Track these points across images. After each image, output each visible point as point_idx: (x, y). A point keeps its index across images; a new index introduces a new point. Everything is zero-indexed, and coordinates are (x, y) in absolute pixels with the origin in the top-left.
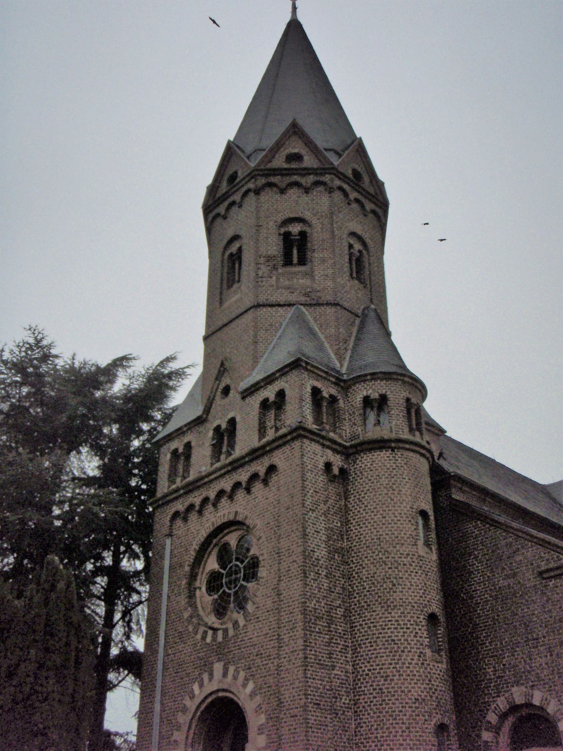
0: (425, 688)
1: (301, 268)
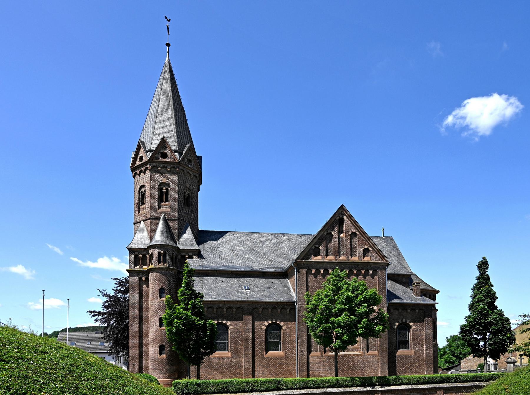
1: (167, 203)
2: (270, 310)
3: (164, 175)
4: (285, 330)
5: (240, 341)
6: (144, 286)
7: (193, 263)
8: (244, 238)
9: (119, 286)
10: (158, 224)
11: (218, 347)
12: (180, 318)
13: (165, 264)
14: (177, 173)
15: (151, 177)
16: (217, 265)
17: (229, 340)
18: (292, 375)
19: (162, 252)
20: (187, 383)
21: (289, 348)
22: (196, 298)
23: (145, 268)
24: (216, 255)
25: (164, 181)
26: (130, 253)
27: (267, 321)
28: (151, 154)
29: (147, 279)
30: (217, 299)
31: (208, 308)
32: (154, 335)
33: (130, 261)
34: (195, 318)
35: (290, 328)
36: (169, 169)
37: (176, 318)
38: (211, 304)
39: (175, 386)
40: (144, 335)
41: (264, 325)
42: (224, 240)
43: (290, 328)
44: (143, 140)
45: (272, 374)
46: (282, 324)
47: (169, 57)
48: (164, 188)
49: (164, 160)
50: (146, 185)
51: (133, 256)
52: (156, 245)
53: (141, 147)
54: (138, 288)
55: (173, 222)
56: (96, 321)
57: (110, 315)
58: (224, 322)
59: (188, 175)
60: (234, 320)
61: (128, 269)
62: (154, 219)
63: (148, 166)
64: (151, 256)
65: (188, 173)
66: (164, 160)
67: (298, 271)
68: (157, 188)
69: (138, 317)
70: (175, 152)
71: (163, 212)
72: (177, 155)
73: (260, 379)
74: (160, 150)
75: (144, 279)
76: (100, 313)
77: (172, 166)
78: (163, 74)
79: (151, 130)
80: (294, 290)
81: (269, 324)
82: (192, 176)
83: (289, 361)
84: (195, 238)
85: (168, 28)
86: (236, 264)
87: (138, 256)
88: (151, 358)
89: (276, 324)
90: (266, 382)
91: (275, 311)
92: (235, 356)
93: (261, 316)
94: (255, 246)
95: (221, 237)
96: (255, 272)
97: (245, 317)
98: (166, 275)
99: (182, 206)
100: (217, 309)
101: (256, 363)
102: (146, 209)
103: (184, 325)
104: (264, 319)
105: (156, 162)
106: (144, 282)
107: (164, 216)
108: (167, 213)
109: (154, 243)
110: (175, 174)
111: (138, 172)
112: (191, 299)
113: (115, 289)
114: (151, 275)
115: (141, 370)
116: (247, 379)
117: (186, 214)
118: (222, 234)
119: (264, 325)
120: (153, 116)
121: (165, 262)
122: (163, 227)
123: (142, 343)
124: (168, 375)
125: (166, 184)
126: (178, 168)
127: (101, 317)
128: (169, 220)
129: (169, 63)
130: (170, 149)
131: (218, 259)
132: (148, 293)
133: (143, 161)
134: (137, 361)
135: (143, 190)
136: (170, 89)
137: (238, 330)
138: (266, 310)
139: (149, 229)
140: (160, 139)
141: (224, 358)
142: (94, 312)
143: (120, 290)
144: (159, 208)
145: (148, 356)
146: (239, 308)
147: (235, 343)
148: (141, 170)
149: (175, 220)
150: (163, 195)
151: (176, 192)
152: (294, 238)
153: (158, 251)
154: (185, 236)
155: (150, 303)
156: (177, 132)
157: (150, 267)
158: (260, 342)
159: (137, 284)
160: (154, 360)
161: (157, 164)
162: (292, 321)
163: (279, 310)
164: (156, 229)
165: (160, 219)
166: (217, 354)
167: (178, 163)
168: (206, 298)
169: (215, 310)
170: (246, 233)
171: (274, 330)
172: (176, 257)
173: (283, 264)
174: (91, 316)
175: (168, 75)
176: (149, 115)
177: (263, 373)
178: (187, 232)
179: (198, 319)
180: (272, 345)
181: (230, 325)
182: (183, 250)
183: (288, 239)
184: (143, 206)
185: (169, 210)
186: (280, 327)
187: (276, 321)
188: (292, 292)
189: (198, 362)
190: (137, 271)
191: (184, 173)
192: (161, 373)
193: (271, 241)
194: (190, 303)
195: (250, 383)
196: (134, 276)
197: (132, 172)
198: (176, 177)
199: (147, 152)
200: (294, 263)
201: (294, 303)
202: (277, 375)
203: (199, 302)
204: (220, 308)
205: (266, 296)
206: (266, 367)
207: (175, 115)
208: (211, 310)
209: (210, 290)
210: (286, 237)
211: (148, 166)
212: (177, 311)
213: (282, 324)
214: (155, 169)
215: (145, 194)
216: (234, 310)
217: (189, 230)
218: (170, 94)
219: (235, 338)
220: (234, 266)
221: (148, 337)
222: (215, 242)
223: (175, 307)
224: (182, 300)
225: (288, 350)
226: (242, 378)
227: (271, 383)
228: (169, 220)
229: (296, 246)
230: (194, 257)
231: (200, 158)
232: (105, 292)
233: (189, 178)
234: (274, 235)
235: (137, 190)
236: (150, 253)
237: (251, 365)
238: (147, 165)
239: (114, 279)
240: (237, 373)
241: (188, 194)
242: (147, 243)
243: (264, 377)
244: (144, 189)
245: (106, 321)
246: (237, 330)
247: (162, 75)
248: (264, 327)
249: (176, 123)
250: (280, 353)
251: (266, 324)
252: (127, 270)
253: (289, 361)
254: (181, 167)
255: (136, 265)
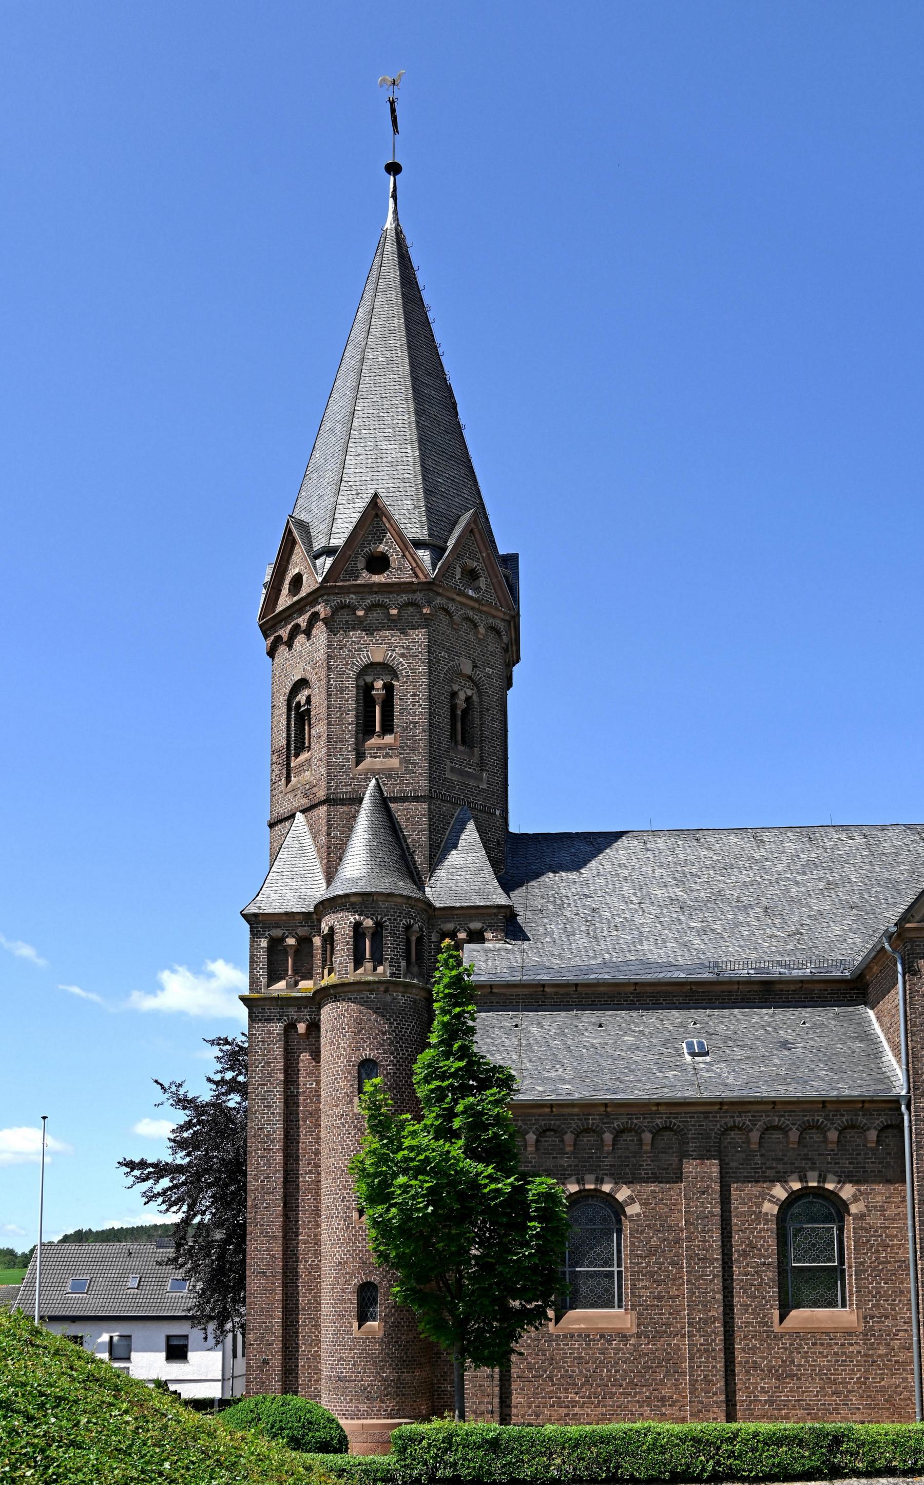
0: (348, 1251)
1: (389, 739)
2: (794, 1135)
3: (378, 636)
4: (861, 1217)
5: (674, 1264)
6: (305, 1057)
7: (488, 960)
8: (685, 851)
9: (231, 1068)
10: (355, 817)
11: (584, 1290)
12: (420, 1171)
13: (380, 969)
14: (427, 622)
15: (330, 645)
16: (577, 961)
17: (627, 1262)
18: (897, 1412)
19: (369, 923)
20: (449, 1439)
21: (878, 1294)
22: (484, 1085)
23: (307, 986)
24: (578, 925)
25: (379, 658)
26: (254, 935)
27: (782, 1179)
28: (329, 561)
29: (314, 1027)
30: (577, 1096)
31: (542, 1133)
32: (340, 1241)
33: (252, 962)
34: (481, 1167)
35: (883, 1209)
36: (394, 612)
37: (405, 1172)
38: (553, 1118)
39: (402, 1450)
40: (302, 1247)
41: (773, 1199)
42: (608, 867)
43: (883, 1209)
44: (303, 516)
45: (808, 1408)
46: (847, 1192)
47: (395, 211)
48: (379, 684)
49: (376, 579)
50: (313, 678)
51: (264, 943)
52: (347, 896)
53: (294, 542)
54: (280, 1065)
55: (412, 805)
56: (150, 1197)
57: (198, 1176)
58: (607, 1188)
59: (466, 626)
60: (646, 1180)
61: (247, 993)
62: (342, 802)
63: (322, 609)
64: (329, 939)
65: (467, 619)
66: (376, 579)
67: (910, 970)
68: (350, 684)
69: (280, 1175)
70: (418, 544)
71: (373, 773)
72: (424, 555)
73: (752, 1427)
74: (362, 546)
75: (302, 1027)
76: (161, 1170)
77: (405, 598)
78: (375, 273)
79: (330, 476)
80: (895, 1048)
81: (794, 1197)
82: (482, 630)
83: (882, 1350)
84: (495, 864)
85: (393, 110)
86: (653, 952)
87: (282, 942)
88: (327, 1333)
89: (820, 1193)
90: (778, 1440)
91: (817, 1137)
92: (652, 1329)
93: (758, 1160)
94: (731, 884)
95: (593, 856)
96: (730, 982)
97: (691, 1167)
98: (381, 1010)
99: (445, 744)
100: (578, 1135)
101: (739, 1357)
102: (313, 768)
103: (433, 1195)
104: (769, 1173)
105: (347, 590)
106: (302, 1042)
107: (378, 786)
108: (389, 776)
109: (338, 889)
110: (418, 637)
111: (284, 633)
112: (465, 1090)
113: (217, 1078)
114: (328, 1013)
115: (289, 1382)
116: (696, 1427)
117: (461, 773)
118: (598, 842)
119: (773, 1199)
120: (339, 427)
121: (378, 960)
122: (374, 829)
123: (297, 1275)
124: (390, 1405)
125: (385, 668)
126: (429, 602)
127: (165, 1183)
128: (395, 799)
129: (398, 233)
130: (400, 535)
131: (581, 941)
132: (318, 1083)
133: (303, 593)
134: (277, 1346)
135: (301, 697)
136: (399, 322)
137: (664, 1218)
138: (776, 1136)
139: (323, 839)
140: (361, 505)
141: (606, 1337)
142: (143, 1164)
143: (234, 1079)
144: (360, 757)
145: (317, 1326)
146: (666, 1128)
147: (652, 1274)
148: (297, 626)
149: (416, 799)
150: (373, 710)
151: (423, 695)
152: (891, 841)
153: (352, 918)
154: (454, 858)
155: (324, 1121)
156: (426, 471)
157: (323, 983)
158: (757, 1268)
159: (278, 1050)
160: (339, 1343)
161: (351, 599)
162: (889, 1181)
163: (833, 1135)
164: (349, 837)
165: (360, 800)
166: (580, 1318)
167: (429, 586)
168: (530, 1089)
169: (569, 1138)
170: (694, 834)
171: (812, 1220)
172: (419, 940)
173: (845, 944)
174: (131, 1180)
175: (392, 272)
176: (327, 425)
177: (771, 1401)
178: (462, 843)
179: (490, 1170)
180: (805, 1282)
181: (631, 1200)
182: (449, 912)
183: (868, 846)
184: (304, 756)
185: (394, 762)
186: (839, 1209)
187: (822, 1179)
188: (889, 1056)
189: (497, 1353)
190: (278, 998)
191: (452, 622)
192: (365, 1395)
193: (795, 858)
194: (460, 1108)
195: (709, 1443)
196: (269, 1020)
197: (266, 636)
198: (419, 637)
199: (317, 557)
200: (890, 937)
201: (895, 1102)
202: (830, 1412)
203: (497, 1102)
204: (587, 1130)
205: (783, 1080)
206: (782, 1374)
207: (419, 413)
208: (551, 1139)
209: (546, 1061)
210: (859, 839)
211: (320, 608)
212: (407, 1143)
213: (847, 1192)
214: (344, 616)
215: (308, 711)
216: (647, 1137)
217: (470, 835)
218: (399, 340)
219: (651, 1253)
220: (646, 964)
221: (317, 1254)
222: (571, 876)
223: (402, 1126)
224: (428, 1099)
225: (877, 1306)
226: (683, 1420)
227: (801, 1443)
228: (395, 799)
229: (901, 872)
230: (489, 935)
231: (511, 561)
232: (182, 1091)
233: (471, 637)
234: (808, 833)
235: (282, 701)
236: (325, 929)
237: (720, 1366)
238: (315, 603)
239: (212, 1043)
240: (663, 1401)
241: (468, 699)
242: (319, 891)
243: (771, 1419)
244: (306, 692)
245: (180, 1201)
246: (658, 1221)
247: (373, 278)
248: (770, 1208)
249: (420, 441)
250: (844, 1317)
251: (779, 1192)
252: (243, 999)
253: (882, 1350)
254: (439, 600)
255: (273, 978)
